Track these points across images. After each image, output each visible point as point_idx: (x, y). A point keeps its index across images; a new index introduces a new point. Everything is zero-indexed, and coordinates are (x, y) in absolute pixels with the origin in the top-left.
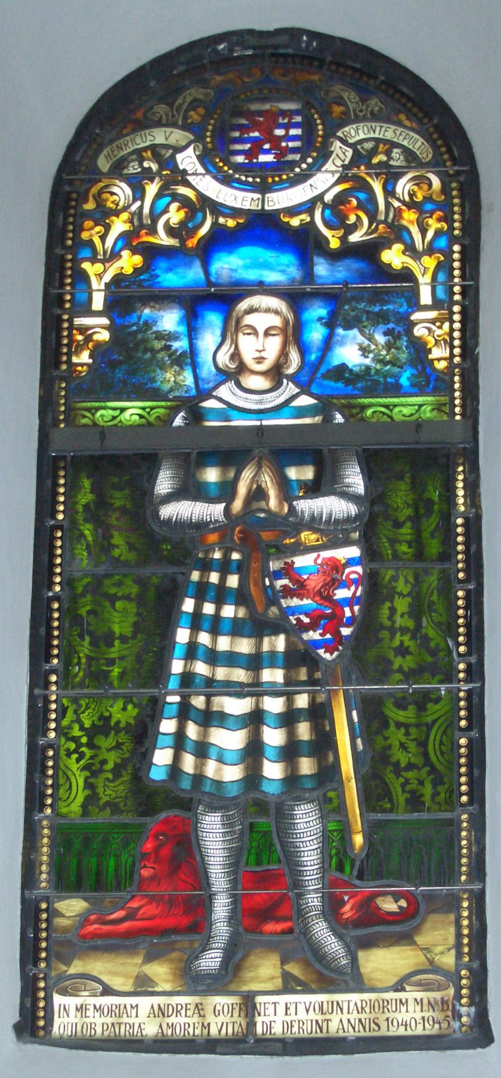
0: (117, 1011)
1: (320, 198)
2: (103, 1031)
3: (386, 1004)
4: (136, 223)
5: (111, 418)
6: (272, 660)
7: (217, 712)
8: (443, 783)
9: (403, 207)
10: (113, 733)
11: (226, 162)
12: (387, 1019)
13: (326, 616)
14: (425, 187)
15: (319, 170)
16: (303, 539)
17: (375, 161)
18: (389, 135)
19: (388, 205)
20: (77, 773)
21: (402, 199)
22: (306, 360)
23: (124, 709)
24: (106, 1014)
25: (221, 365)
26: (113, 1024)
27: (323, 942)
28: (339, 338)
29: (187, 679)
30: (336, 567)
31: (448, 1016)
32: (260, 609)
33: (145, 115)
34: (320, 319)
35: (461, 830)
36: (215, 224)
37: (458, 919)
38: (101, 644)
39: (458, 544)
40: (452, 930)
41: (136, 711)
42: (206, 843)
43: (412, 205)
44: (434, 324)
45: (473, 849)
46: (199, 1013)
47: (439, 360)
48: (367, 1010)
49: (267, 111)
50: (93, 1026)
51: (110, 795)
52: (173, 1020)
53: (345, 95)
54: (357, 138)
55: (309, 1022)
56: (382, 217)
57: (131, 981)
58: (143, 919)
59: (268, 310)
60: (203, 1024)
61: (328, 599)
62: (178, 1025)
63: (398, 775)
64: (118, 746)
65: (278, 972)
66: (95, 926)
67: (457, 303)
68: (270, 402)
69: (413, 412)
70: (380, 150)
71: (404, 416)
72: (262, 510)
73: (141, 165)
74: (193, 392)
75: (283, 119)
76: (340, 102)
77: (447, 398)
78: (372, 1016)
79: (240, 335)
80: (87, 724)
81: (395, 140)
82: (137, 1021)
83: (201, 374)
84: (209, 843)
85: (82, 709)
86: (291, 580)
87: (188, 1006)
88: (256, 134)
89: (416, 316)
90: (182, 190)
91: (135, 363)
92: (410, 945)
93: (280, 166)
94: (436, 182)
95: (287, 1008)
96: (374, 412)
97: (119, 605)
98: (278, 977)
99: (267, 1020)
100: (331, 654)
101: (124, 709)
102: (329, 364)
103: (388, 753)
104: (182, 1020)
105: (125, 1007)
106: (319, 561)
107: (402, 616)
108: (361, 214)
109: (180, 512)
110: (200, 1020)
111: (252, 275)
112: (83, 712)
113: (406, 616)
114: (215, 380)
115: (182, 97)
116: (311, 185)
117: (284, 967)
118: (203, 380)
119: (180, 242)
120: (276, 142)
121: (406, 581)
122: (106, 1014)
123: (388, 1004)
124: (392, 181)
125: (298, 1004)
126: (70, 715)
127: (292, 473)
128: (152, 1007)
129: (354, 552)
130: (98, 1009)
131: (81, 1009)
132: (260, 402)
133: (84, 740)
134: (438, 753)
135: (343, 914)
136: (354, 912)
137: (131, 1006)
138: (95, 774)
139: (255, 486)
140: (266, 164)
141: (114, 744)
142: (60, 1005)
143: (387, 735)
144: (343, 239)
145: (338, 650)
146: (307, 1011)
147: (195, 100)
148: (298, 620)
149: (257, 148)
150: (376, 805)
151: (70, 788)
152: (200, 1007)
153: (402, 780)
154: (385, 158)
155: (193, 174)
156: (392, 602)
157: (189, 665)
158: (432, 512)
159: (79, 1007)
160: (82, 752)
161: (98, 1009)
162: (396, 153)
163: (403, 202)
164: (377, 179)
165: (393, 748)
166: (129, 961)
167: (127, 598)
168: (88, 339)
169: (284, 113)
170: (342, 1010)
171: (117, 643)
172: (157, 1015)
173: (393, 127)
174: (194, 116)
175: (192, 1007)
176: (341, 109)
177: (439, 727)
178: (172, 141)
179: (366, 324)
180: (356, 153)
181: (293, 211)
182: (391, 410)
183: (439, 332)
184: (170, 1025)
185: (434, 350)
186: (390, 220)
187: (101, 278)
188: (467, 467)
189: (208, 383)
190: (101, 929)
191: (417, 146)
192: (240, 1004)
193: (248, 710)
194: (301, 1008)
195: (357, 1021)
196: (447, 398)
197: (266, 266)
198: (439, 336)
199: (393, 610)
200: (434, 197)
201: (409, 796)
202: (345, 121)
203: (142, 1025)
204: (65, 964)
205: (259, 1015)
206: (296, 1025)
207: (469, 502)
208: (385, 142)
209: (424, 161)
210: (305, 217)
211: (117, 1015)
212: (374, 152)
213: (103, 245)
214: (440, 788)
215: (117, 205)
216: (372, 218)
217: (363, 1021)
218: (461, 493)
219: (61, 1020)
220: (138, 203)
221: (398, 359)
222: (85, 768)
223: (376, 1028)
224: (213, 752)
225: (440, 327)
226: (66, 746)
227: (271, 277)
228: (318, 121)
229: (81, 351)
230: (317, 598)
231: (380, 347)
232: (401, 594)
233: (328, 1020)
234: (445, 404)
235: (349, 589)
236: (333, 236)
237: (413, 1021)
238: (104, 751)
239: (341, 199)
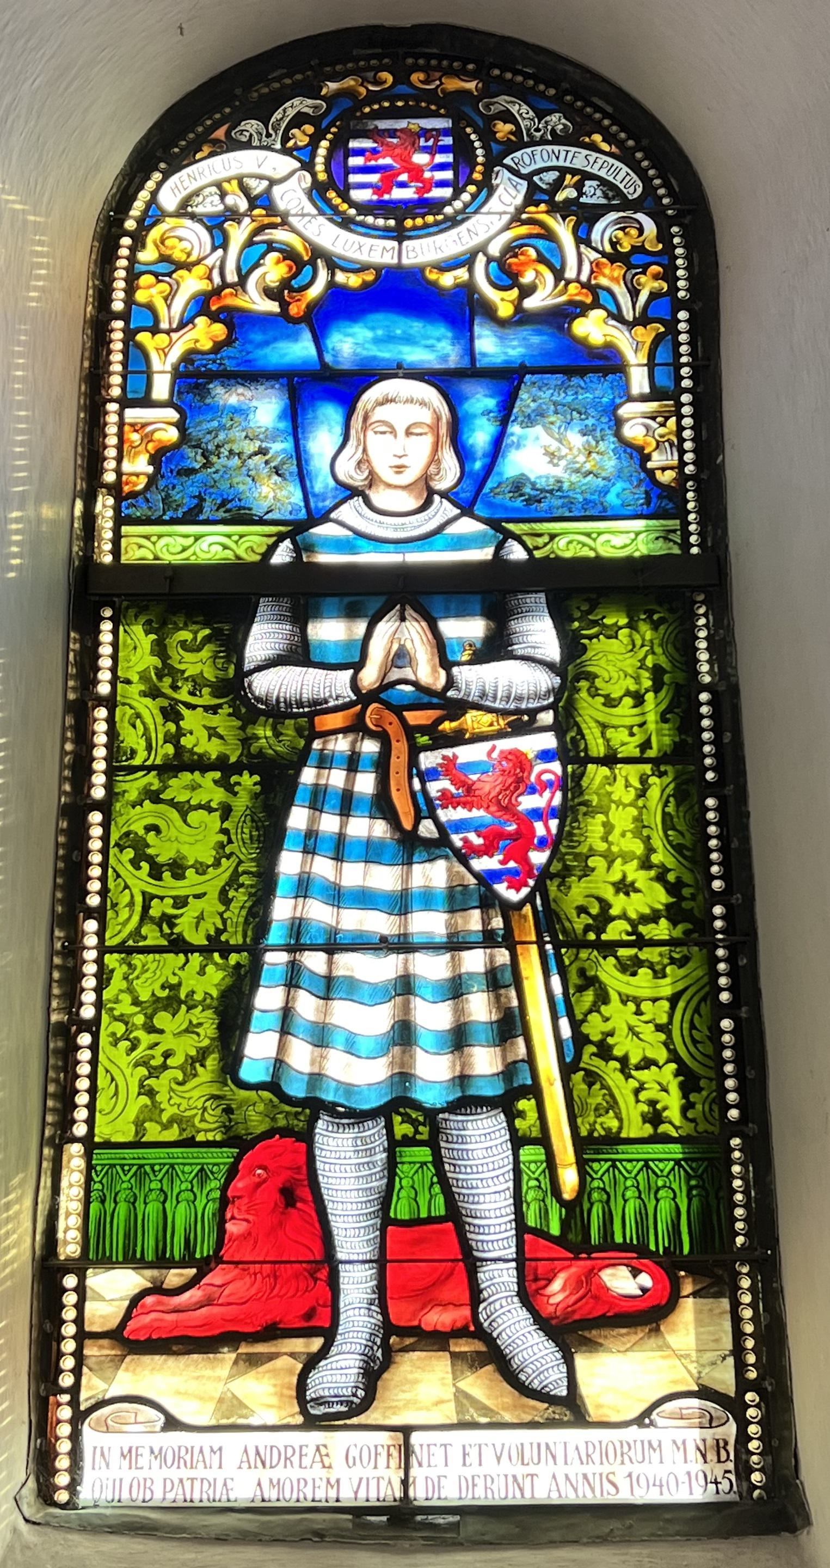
0: (188, 1458)
1: (482, 248)
2: (165, 1493)
3: (626, 1448)
4: (217, 280)
5: (180, 549)
6: (427, 900)
7: (345, 977)
8: (699, 1090)
9: (604, 260)
10: (184, 1008)
11: (346, 198)
12: (630, 1475)
13: (509, 836)
14: (634, 232)
16: (469, 722)
17: (560, 197)
18: (579, 163)
20: (128, 1072)
22: (467, 469)
23: (202, 972)
24: (169, 1462)
25: (341, 476)
26: (181, 1481)
27: (520, 1342)
28: (514, 439)
29: (297, 927)
30: (519, 761)
31: (729, 1472)
32: (407, 825)
33: (228, 133)
34: (487, 413)
35: (731, 1162)
36: (331, 284)
37: (735, 1305)
38: (167, 875)
39: (704, 730)
40: (727, 1325)
41: (221, 974)
42: (330, 1181)
43: (615, 257)
44: (654, 419)
45: (753, 1194)
46: (322, 1461)
47: (663, 469)
48: (596, 1457)
49: (402, 130)
50: (149, 1483)
51: (179, 1105)
52: (279, 1473)
53: (514, 109)
54: (534, 167)
55: (503, 1479)
56: (570, 273)
57: (211, 1406)
58: (229, 1304)
59: (410, 401)
60: (328, 1481)
61: (509, 810)
62: (288, 1482)
63: (628, 1076)
64: (191, 1029)
65: (449, 1393)
66: (153, 1316)
67: (686, 390)
68: (415, 527)
69: (628, 542)
70: (566, 183)
71: (613, 547)
72: (406, 682)
74: (303, 514)
75: (427, 141)
76: (507, 117)
77: (678, 522)
78: (606, 1469)
79: (370, 434)
80: (144, 996)
81: (588, 169)
82: (220, 1476)
83: (312, 487)
84: (333, 1181)
85: (136, 973)
86: (453, 782)
87: (304, 1451)
88: (388, 161)
90: (280, 235)
91: (216, 472)
92: (660, 1348)
93: (424, 205)
94: (650, 227)
95: (465, 1455)
96: (570, 542)
97: (193, 817)
98: (449, 1401)
99: (433, 1473)
100: (518, 890)
101: (202, 972)
102: (500, 474)
103: (610, 1040)
104: (294, 1473)
105: (201, 1451)
106: (495, 755)
107: (623, 835)
108: (542, 268)
109: (285, 682)
110: (324, 1473)
111: (386, 354)
112: (138, 978)
113: (629, 835)
114: (334, 497)
115: (280, 110)
116: (469, 230)
117: (458, 1385)
118: (315, 495)
119: (280, 306)
120: (416, 173)
121: (628, 785)
122: (169, 1462)
123: (630, 1448)
124: (584, 225)
125: (483, 1447)
126: (117, 983)
127: (452, 628)
128: (246, 1451)
129: (548, 741)
130: (158, 1454)
131: (129, 1454)
132: (403, 527)
133: (140, 1020)
134: (688, 1040)
135: (549, 1297)
136: (567, 1293)
137: (212, 1450)
138: (155, 1072)
139: (395, 647)
140: (405, 203)
141: (184, 1027)
142: (95, 1448)
143: (607, 1015)
145: (526, 885)
146: (499, 1459)
147: (299, 113)
148: (465, 840)
149: (389, 180)
150: (595, 1122)
151: (116, 1094)
152: (323, 1451)
153: (633, 1084)
154: (574, 194)
155: (296, 215)
156: (607, 815)
157: (300, 908)
158: (663, 684)
159: (126, 1452)
160: (136, 1038)
161: (158, 1454)
162: (589, 185)
163: (604, 254)
164: (564, 220)
165: (617, 1033)
166: (208, 1373)
167: (208, 808)
168: (148, 438)
169: (425, 133)
170: (554, 1457)
171: (190, 873)
172: (253, 1465)
173: (585, 152)
174: (300, 137)
175: (311, 1451)
176: (509, 127)
177: (688, 1003)
178: (266, 171)
179: (552, 419)
180: (533, 188)
181: (445, 267)
182: (594, 540)
183: (662, 430)
184: (275, 1482)
185: (655, 456)
186: (584, 278)
187: (166, 355)
188: (711, 617)
189: (324, 500)
190: (161, 1320)
191: (619, 178)
192: (389, 1447)
193: (392, 975)
194: (488, 1454)
195: (580, 1478)
196: (678, 522)
197: (408, 340)
198: (662, 436)
199: (608, 827)
200: (647, 246)
201: (645, 1108)
202: (517, 143)
203: (229, 1482)
204: (104, 1379)
205: (420, 1465)
206: (480, 1482)
207: (716, 670)
208: (574, 172)
209: (630, 197)
210: (462, 274)
211: (189, 1465)
212: (558, 185)
214: (693, 1097)
215: (189, 255)
216: (559, 275)
217: (590, 1477)
218: (704, 656)
219: (97, 1473)
221: (602, 468)
222: (143, 1063)
223: (613, 1491)
224: (339, 1039)
225: (663, 425)
226: (110, 1030)
227: (415, 355)
228: (477, 144)
229: (137, 454)
230: (493, 809)
231: (575, 452)
232: (619, 803)
233: (532, 1475)
234: (674, 531)
235: (541, 795)
236: (503, 300)
237: (672, 1478)
238: (171, 1036)
239: (512, 249)
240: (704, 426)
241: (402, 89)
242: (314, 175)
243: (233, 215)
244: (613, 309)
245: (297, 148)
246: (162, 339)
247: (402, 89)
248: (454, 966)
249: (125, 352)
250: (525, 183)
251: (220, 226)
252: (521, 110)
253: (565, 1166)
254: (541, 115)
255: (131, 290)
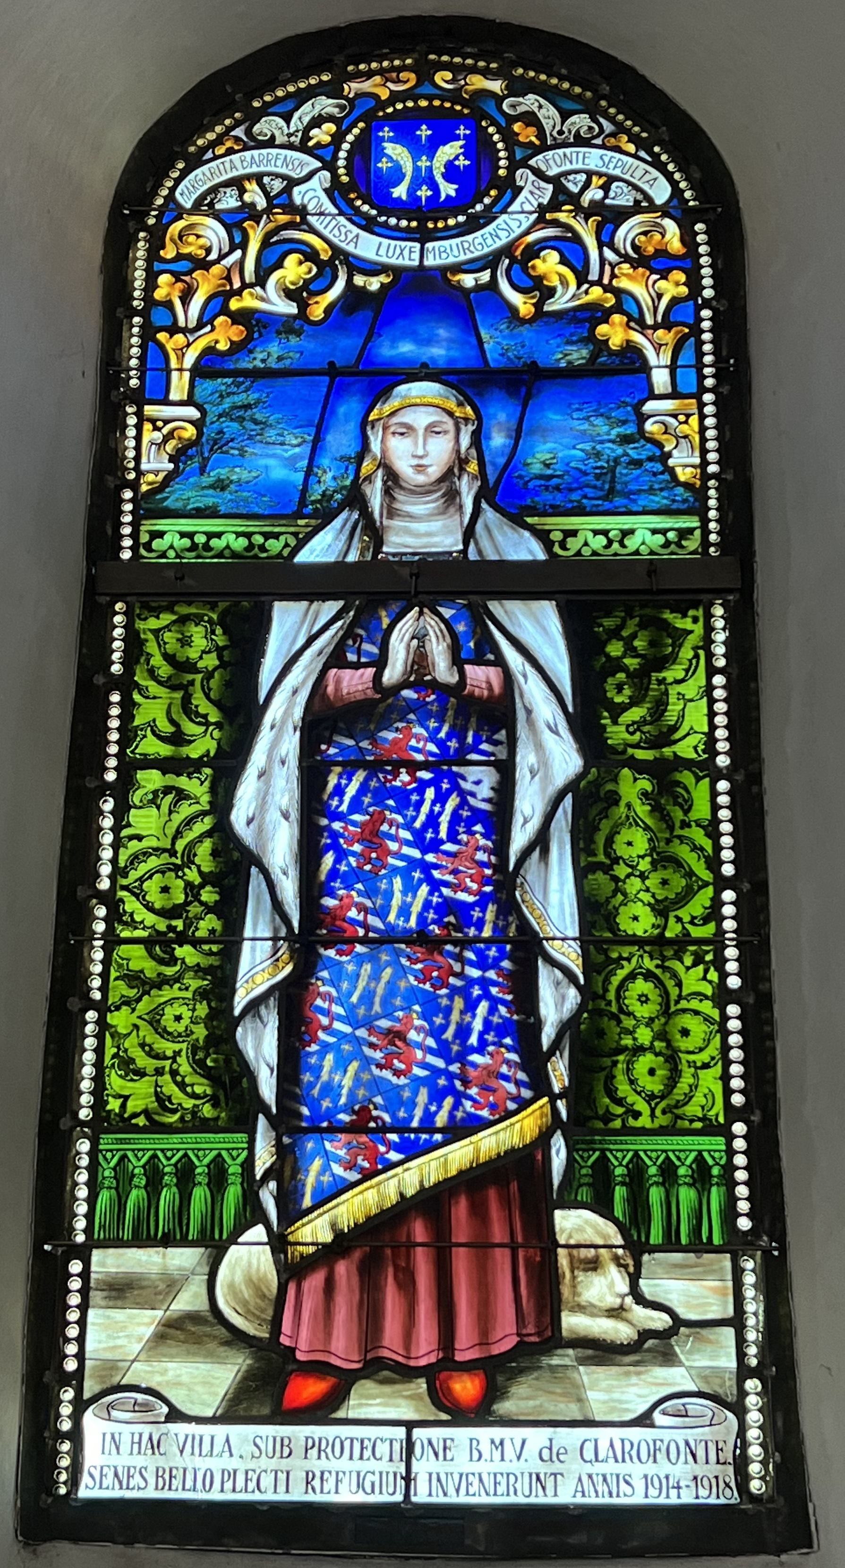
15: (504, 211)
19: (602, 260)
21: (623, 252)
44: (675, 416)
73: (241, 196)
76: (530, 119)
89: (650, 406)
144: (538, 306)
154: (600, 194)
164: (586, 221)
185: (675, 453)
208: (600, 175)
213: (186, 313)
215: (208, 251)
220: (238, 254)
228: (500, 145)
240: (727, 428)
241: (427, 89)
242: (335, 177)
243: (250, 213)
244: (636, 315)
245: (319, 145)
246: (180, 338)
247: (427, 89)
248: (266, 793)
249: (143, 347)
250: (550, 187)
251: (239, 225)
252: (548, 114)
253: (477, 1151)
254: (565, 115)
255: (151, 284)
